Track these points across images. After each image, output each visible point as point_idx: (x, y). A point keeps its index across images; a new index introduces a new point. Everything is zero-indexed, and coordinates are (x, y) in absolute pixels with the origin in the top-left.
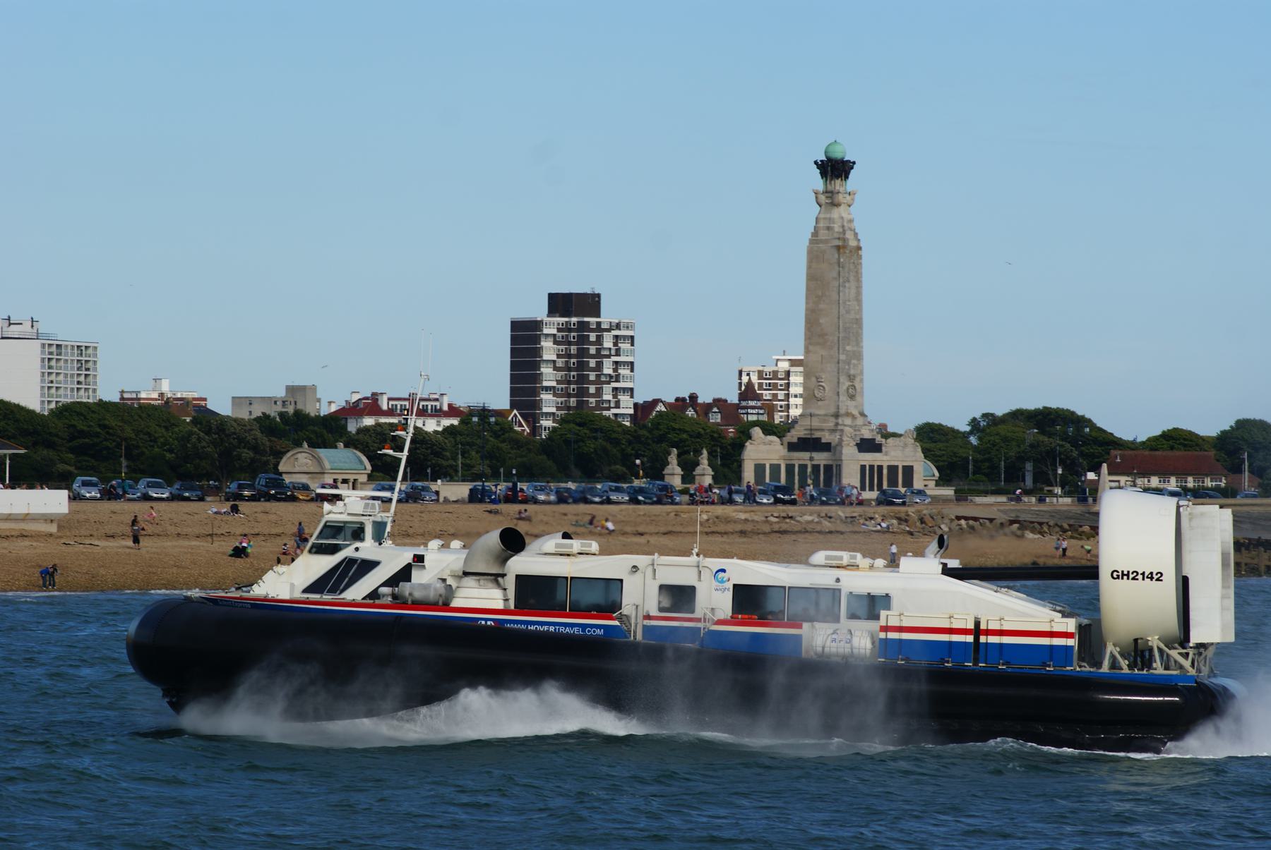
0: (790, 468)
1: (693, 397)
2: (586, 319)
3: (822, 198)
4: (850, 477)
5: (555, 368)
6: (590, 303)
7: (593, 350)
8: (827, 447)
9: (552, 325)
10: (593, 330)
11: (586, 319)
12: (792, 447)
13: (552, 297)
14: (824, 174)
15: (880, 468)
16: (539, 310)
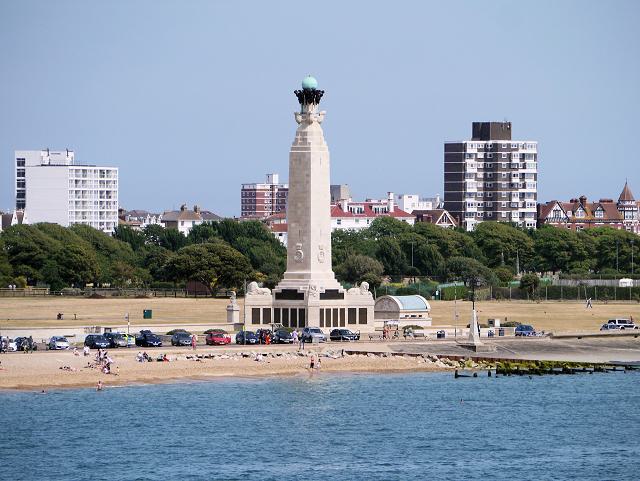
0: (277, 311)
1: (583, 200)
2: (499, 142)
3: (300, 118)
4: (313, 322)
5: (477, 179)
6: (505, 130)
7: (504, 163)
8: (300, 296)
9: (474, 147)
10: (504, 150)
11: (499, 142)
12: (279, 296)
13: (475, 125)
14: (301, 101)
15: (343, 310)
16: (464, 136)
